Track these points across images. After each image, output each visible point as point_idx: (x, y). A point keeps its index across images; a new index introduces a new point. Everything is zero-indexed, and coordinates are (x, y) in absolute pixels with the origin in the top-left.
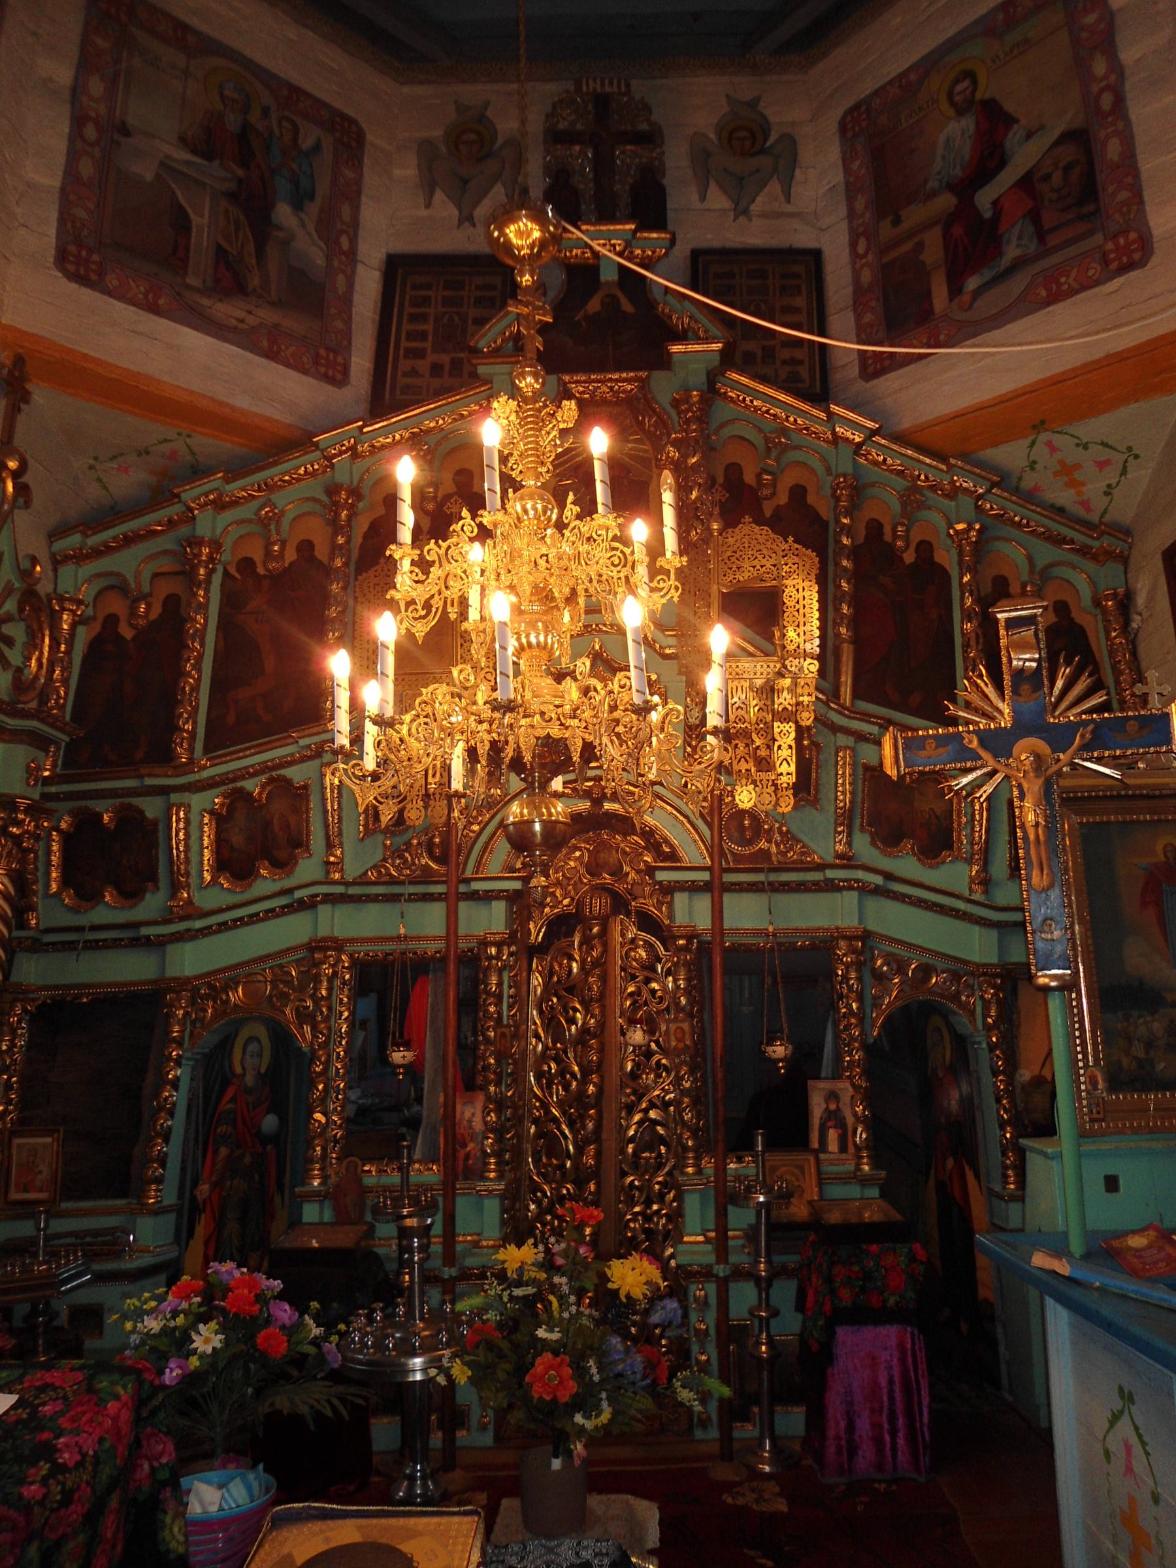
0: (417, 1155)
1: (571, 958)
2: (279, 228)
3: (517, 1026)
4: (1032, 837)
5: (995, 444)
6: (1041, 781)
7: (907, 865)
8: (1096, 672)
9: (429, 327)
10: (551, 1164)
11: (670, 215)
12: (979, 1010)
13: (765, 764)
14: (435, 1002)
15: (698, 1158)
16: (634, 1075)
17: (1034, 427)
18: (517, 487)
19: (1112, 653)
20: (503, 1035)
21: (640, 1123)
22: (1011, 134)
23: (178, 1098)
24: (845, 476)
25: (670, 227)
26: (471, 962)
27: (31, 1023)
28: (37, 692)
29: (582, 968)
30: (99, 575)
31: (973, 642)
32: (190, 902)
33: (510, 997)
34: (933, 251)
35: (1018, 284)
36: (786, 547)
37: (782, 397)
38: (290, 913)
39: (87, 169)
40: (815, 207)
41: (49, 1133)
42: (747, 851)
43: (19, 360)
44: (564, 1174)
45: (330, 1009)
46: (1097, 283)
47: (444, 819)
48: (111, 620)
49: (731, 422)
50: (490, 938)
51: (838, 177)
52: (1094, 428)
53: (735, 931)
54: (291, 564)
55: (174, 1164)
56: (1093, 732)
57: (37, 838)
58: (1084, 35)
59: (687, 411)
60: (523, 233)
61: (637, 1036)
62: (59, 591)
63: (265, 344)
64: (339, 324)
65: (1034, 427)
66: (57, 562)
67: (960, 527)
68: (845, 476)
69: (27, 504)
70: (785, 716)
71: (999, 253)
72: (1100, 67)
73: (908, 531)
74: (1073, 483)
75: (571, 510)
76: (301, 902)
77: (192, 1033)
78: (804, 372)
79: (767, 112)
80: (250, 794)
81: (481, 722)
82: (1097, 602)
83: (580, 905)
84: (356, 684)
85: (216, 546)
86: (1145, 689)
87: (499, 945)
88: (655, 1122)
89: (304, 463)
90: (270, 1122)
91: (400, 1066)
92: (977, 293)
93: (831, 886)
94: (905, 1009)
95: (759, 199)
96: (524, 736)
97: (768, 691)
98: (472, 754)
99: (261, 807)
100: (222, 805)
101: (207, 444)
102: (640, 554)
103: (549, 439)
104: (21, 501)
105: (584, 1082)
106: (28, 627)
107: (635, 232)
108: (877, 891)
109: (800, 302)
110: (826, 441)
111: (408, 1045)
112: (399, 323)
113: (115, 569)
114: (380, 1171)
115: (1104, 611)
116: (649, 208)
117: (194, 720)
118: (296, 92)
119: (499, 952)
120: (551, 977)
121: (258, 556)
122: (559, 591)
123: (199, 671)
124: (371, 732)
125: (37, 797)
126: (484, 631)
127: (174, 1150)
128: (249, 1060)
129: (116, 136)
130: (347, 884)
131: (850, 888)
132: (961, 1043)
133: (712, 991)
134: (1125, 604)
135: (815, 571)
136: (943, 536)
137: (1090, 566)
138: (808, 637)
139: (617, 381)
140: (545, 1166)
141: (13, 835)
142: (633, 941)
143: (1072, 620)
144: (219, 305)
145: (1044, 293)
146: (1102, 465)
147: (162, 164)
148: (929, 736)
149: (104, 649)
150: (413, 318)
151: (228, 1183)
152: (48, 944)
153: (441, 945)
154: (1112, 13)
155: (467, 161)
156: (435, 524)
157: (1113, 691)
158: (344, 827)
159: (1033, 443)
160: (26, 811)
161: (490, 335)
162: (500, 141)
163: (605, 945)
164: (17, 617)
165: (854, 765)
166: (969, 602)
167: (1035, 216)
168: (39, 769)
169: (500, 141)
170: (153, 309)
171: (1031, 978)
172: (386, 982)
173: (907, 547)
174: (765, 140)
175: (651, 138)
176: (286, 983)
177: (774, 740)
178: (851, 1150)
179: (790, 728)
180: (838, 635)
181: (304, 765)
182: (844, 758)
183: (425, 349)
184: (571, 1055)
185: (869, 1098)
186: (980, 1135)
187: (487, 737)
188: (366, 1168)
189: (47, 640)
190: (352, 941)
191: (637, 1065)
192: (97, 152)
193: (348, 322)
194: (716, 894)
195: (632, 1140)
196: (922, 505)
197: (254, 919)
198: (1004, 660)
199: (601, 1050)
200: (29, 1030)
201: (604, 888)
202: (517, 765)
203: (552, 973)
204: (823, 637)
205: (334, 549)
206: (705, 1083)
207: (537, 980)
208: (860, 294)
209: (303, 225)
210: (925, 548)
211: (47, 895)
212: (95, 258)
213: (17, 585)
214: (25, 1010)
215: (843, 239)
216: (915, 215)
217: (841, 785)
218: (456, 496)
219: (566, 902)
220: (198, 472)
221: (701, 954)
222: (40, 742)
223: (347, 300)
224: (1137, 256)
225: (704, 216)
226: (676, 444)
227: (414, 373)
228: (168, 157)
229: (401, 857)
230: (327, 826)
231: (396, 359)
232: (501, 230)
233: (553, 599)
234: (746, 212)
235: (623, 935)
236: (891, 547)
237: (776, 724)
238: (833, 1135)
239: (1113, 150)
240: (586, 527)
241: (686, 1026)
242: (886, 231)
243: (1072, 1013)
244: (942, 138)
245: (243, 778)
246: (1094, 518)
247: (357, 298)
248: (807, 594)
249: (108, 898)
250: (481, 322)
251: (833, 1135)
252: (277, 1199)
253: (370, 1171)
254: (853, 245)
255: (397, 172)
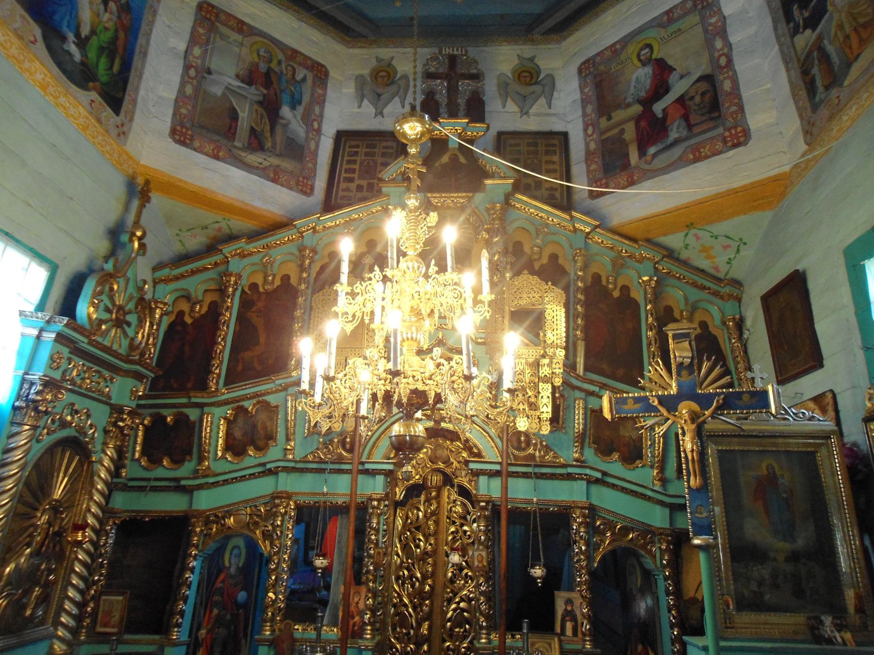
0: (325, 622)
1: (419, 510)
2: (283, 118)
3: (386, 548)
4: (690, 458)
5: (665, 235)
6: (694, 426)
7: (616, 467)
8: (724, 365)
9: (357, 167)
10: (402, 632)
11: (487, 115)
12: (658, 555)
13: (533, 406)
14: (342, 532)
15: (488, 634)
16: (452, 581)
17: (687, 226)
18: (404, 255)
19: (732, 351)
20: (379, 553)
21: (454, 610)
22: (672, 76)
23: (193, 578)
24: (580, 249)
25: (487, 121)
26: (362, 510)
27: (117, 530)
28: (139, 351)
29: (425, 516)
30: (176, 290)
31: (653, 342)
32: (209, 467)
33: (384, 531)
34: (630, 132)
35: (677, 151)
36: (547, 287)
37: (546, 207)
38: (263, 476)
39: (189, 90)
40: (565, 109)
41: (122, 594)
42: (522, 454)
43: (147, 182)
44: (409, 639)
45: (281, 533)
46: (720, 153)
47: (352, 429)
48: (181, 314)
49: (516, 220)
50: (374, 496)
51: (577, 96)
52: (722, 228)
53: (514, 500)
54: (278, 287)
55: (188, 615)
56: (723, 399)
57: (132, 429)
58: (710, 28)
59: (493, 214)
60: (412, 129)
61: (455, 558)
62: (156, 297)
63: (272, 175)
64: (310, 165)
65: (687, 226)
66: (155, 283)
67: (646, 278)
68: (580, 249)
69: (144, 254)
70: (546, 380)
71: (667, 136)
72: (719, 44)
73: (616, 280)
74: (709, 257)
75: (433, 269)
76: (270, 470)
77: (203, 542)
78: (558, 195)
79: (539, 63)
80: (247, 410)
81: (380, 380)
82: (724, 323)
83: (425, 479)
84: (312, 353)
85: (239, 276)
86: (753, 375)
87: (379, 500)
88: (463, 610)
89: (285, 235)
90: (242, 596)
91: (320, 568)
92: (654, 156)
93: (569, 477)
94: (613, 552)
95: (534, 107)
96: (403, 389)
97: (536, 365)
98: (374, 397)
99: (252, 416)
100: (231, 414)
101: (238, 224)
102: (469, 295)
103: (423, 235)
104: (141, 252)
105: (423, 582)
106: (139, 317)
107: (468, 123)
108: (597, 481)
109: (556, 158)
110: (570, 231)
111: (324, 556)
112: (341, 165)
113: (185, 287)
114: (303, 630)
115: (728, 327)
116: (476, 110)
117: (220, 368)
118: (295, 52)
119: (379, 504)
120: (407, 520)
121: (259, 280)
122: (425, 311)
123: (225, 342)
124: (320, 383)
125: (134, 406)
126: (382, 329)
127: (188, 608)
128: (233, 560)
129: (206, 75)
130: (296, 462)
131: (582, 479)
132: (648, 575)
133: (499, 532)
134: (740, 324)
135: (563, 301)
136: (636, 283)
137: (719, 302)
138: (559, 336)
139: (456, 197)
140: (398, 633)
141: (119, 427)
142: (455, 501)
143: (710, 332)
144: (250, 156)
145: (692, 157)
146: (726, 247)
147: (226, 88)
148: (629, 397)
149: (176, 329)
150: (349, 162)
151: (217, 630)
152: (131, 487)
153: (347, 499)
154: (724, 18)
155: (381, 83)
156: (358, 270)
157: (735, 377)
158: (296, 430)
159: (686, 235)
160: (128, 414)
161: (390, 172)
162: (398, 76)
163: (438, 503)
164: (134, 311)
165: (585, 408)
166: (650, 320)
167: (686, 117)
168: (137, 391)
169: (398, 76)
170: (216, 157)
171: (689, 539)
172: (312, 518)
173: (615, 288)
174: (538, 77)
175: (477, 77)
176: (257, 516)
177: (539, 393)
178: (580, 635)
179: (549, 387)
180: (575, 336)
181: (277, 395)
182: (579, 404)
183: (354, 178)
184: (416, 567)
185: (591, 604)
186: (658, 630)
187: (383, 388)
188: (296, 627)
189: (148, 324)
190: (297, 494)
191: (454, 575)
192: (195, 82)
193: (315, 164)
194: (504, 478)
195: (449, 620)
196: (623, 266)
197: (243, 478)
198: (672, 356)
199: (434, 565)
200: (116, 534)
201: (438, 470)
202: (399, 404)
203: (407, 517)
204: (567, 337)
205: (301, 280)
206: (494, 589)
207: (399, 522)
208: (589, 156)
209: (295, 117)
210: (625, 289)
211: (133, 460)
212: (190, 132)
213: (135, 295)
214: (114, 523)
215: (580, 125)
216: (619, 115)
217: (578, 420)
218: (373, 258)
219: (417, 477)
220: (232, 238)
221: (494, 512)
222: (138, 376)
223: (315, 155)
224: (742, 140)
225: (505, 116)
226: (488, 231)
227: (348, 190)
228: (229, 84)
229: (327, 448)
230: (287, 429)
231: (339, 182)
232: (401, 126)
233: (421, 314)
234: (527, 113)
235: (449, 498)
236: (606, 288)
237: (541, 384)
238: (569, 625)
239: (727, 86)
240: (441, 278)
241: (484, 554)
242: (604, 122)
243: (713, 561)
244: (634, 77)
245: (244, 400)
246: (721, 275)
247: (320, 152)
248: (558, 313)
249: (165, 463)
250: (386, 165)
251: (569, 625)
252: (243, 642)
253: (298, 629)
254: (585, 130)
255: (344, 91)
